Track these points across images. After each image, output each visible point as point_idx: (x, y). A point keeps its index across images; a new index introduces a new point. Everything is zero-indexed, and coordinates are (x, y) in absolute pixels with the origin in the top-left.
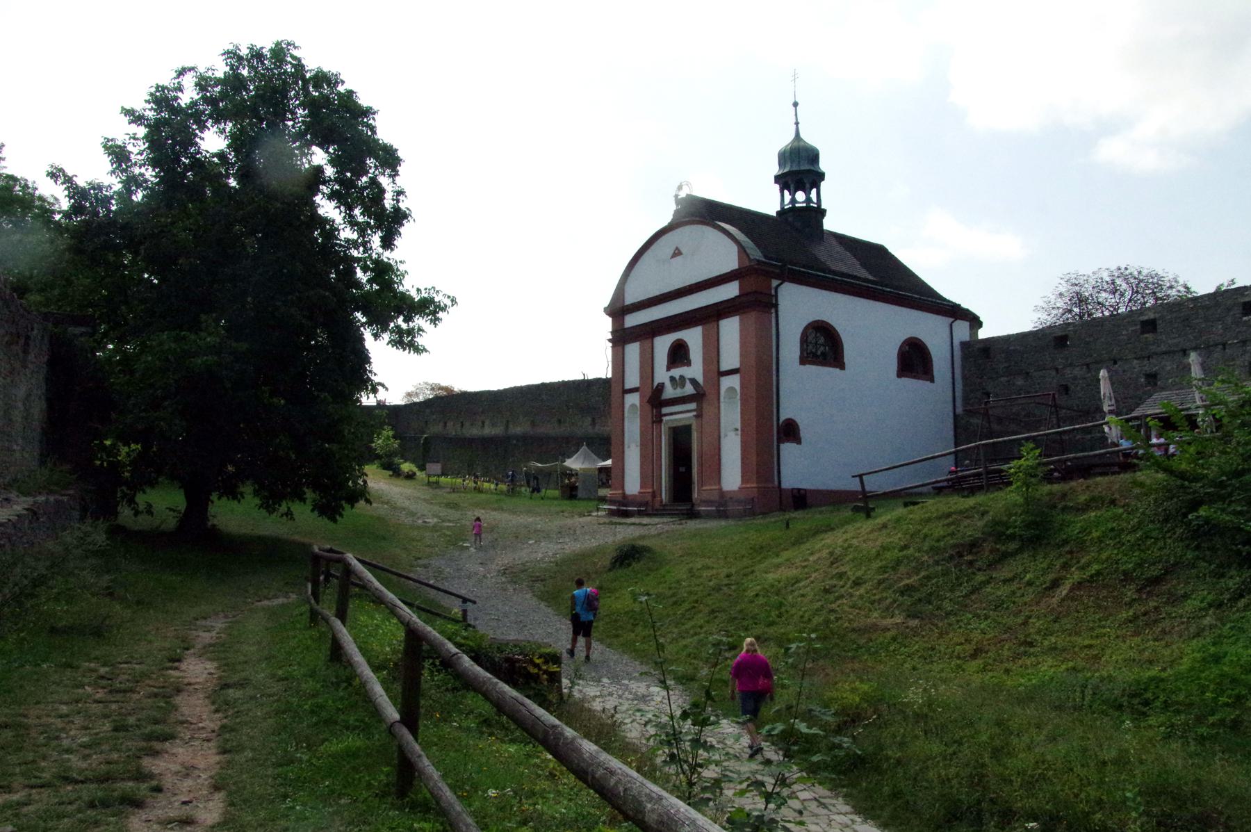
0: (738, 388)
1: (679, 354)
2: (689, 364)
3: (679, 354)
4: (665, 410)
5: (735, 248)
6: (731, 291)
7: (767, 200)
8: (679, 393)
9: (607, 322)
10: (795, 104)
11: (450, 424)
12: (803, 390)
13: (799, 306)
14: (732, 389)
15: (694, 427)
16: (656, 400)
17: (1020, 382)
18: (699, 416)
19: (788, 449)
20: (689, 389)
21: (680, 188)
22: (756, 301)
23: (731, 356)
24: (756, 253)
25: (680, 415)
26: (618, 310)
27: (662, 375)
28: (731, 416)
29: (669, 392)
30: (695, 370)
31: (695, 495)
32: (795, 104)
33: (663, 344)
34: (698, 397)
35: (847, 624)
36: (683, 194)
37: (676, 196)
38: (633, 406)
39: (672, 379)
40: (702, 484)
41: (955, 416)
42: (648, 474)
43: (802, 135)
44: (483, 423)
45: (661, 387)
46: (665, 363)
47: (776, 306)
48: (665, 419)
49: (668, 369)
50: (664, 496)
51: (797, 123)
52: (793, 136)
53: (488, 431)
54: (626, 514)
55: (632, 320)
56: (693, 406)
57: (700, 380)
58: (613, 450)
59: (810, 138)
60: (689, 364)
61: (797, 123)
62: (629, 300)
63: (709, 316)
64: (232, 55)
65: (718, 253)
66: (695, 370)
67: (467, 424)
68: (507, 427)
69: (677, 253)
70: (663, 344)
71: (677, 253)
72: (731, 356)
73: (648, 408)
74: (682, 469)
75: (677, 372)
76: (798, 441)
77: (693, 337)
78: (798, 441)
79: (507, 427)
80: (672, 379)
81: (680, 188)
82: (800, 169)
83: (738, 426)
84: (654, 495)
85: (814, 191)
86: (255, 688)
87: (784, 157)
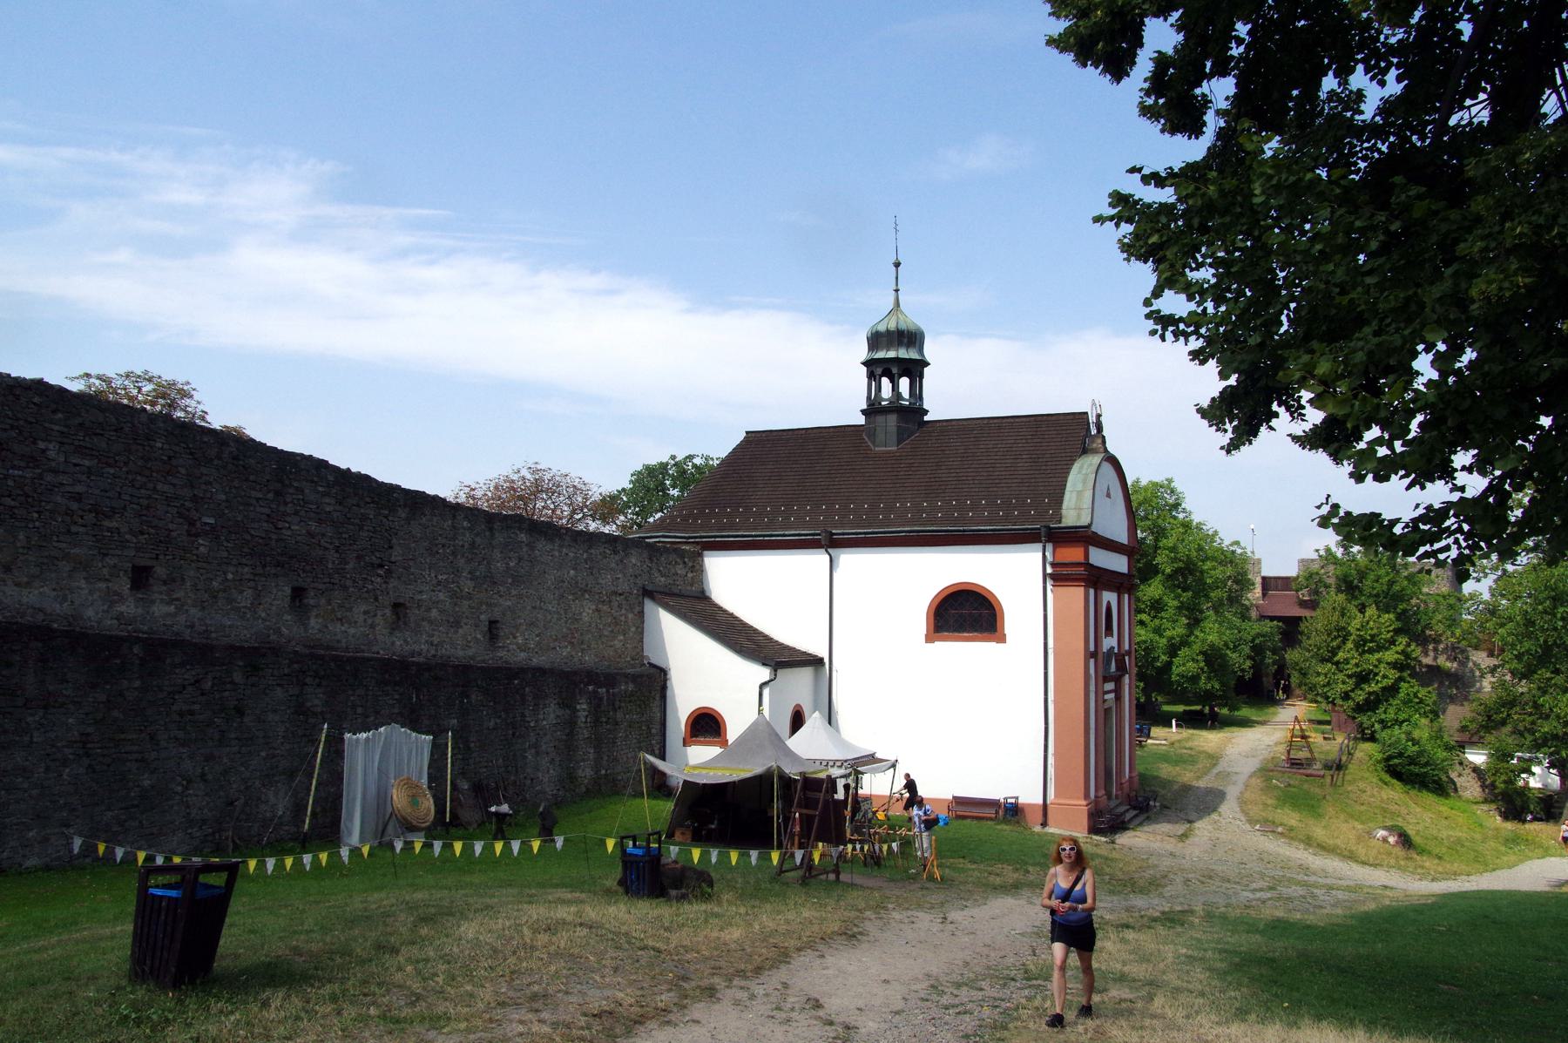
10: (897, 265)
32: (897, 265)
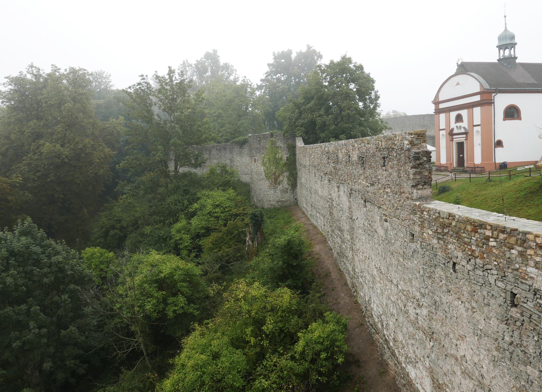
1: (459, 118)
3: (459, 118)
4: (454, 137)
5: (479, 84)
6: (477, 98)
7: (491, 55)
10: (505, 17)
12: (504, 129)
13: (502, 101)
16: (451, 134)
18: (466, 139)
19: (498, 150)
20: (463, 131)
21: (459, 60)
22: (486, 101)
23: (477, 120)
24: (487, 86)
25: (461, 138)
27: (453, 125)
28: (477, 140)
29: (456, 131)
30: (465, 124)
31: (465, 165)
32: (505, 17)
33: (453, 115)
34: (466, 133)
35: (434, 217)
36: (459, 63)
39: (457, 127)
40: (467, 162)
42: (449, 157)
43: (508, 29)
47: (494, 103)
50: (455, 165)
52: (504, 29)
54: (441, 171)
55: (442, 106)
56: (464, 136)
57: (467, 128)
58: (436, 144)
59: (511, 29)
60: (463, 122)
62: (441, 99)
63: (470, 106)
64: (319, 52)
65: (471, 85)
69: (458, 84)
70: (453, 115)
71: (458, 84)
72: (477, 120)
73: (449, 136)
74: (461, 156)
75: (459, 124)
77: (464, 113)
78: (502, 147)
80: (457, 127)
82: (507, 42)
83: (480, 143)
84: (451, 164)
85: (513, 49)
87: (500, 38)
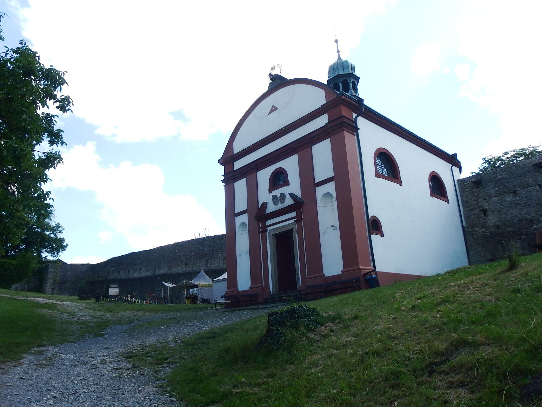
0: (334, 193)
1: (279, 179)
2: (287, 183)
3: (279, 179)
4: (268, 223)
6: (322, 121)
8: (280, 206)
9: (221, 169)
10: (336, 41)
11: (122, 272)
14: (328, 195)
15: (295, 229)
17: (510, 198)
20: (289, 201)
21: (273, 68)
26: (228, 159)
28: (328, 216)
29: (271, 208)
32: (336, 41)
33: (264, 176)
37: (270, 75)
38: (243, 224)
39: (274, 197)
41: (463, 228)
44: (141, 269)
45: (265, 205)
46: (268, 187)
48: (269, 229)
49: (270, 192)
51: (338, 52)
53: (143, 274)
55: (238, 165)
56: (294, 214)
57: (298, 193)
60: (287, 183)
61: (338, 52)
62: (237, 149)
66: (294, 187)
67: (132, 271)
68: (154, 272)
69: (274, 109)
70: (264, 176)
71: (274, 109)
75: (277, 193)
76: (382, 235)
77: (291, 165)
78: (382, 235)
79: (154, 272)
80: (274, 197)
81: (273, 68)
86: (520, 196)
